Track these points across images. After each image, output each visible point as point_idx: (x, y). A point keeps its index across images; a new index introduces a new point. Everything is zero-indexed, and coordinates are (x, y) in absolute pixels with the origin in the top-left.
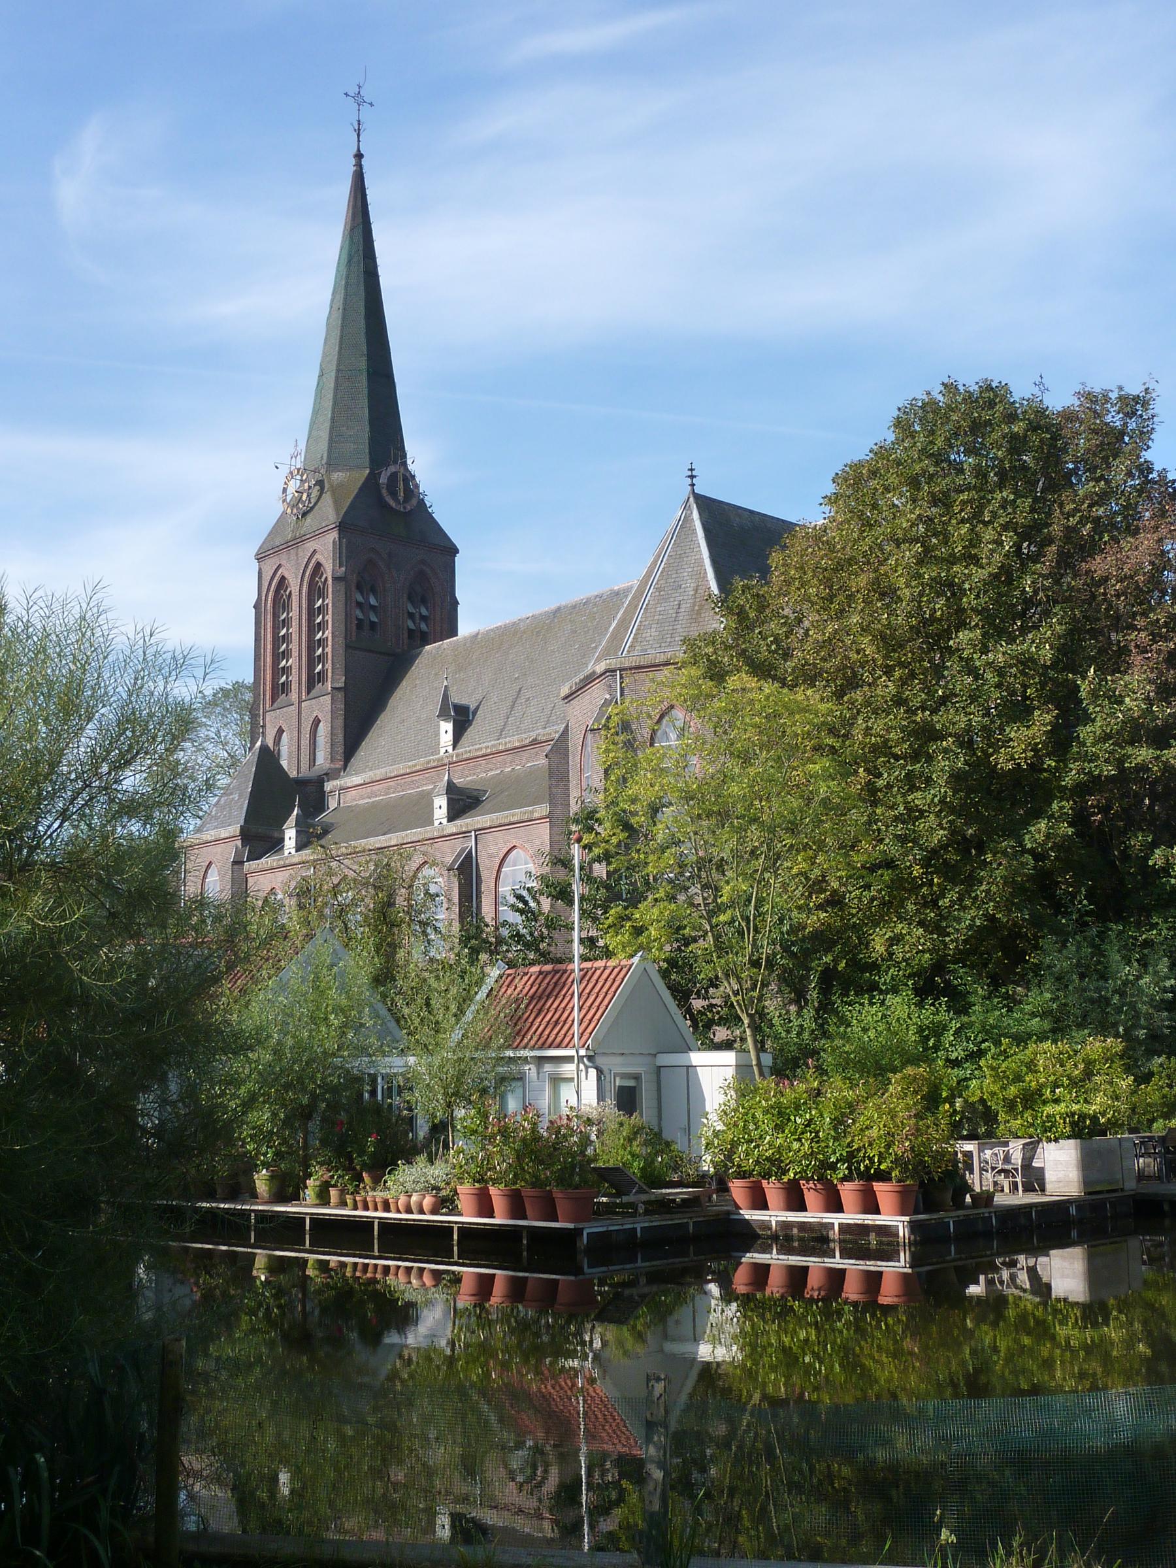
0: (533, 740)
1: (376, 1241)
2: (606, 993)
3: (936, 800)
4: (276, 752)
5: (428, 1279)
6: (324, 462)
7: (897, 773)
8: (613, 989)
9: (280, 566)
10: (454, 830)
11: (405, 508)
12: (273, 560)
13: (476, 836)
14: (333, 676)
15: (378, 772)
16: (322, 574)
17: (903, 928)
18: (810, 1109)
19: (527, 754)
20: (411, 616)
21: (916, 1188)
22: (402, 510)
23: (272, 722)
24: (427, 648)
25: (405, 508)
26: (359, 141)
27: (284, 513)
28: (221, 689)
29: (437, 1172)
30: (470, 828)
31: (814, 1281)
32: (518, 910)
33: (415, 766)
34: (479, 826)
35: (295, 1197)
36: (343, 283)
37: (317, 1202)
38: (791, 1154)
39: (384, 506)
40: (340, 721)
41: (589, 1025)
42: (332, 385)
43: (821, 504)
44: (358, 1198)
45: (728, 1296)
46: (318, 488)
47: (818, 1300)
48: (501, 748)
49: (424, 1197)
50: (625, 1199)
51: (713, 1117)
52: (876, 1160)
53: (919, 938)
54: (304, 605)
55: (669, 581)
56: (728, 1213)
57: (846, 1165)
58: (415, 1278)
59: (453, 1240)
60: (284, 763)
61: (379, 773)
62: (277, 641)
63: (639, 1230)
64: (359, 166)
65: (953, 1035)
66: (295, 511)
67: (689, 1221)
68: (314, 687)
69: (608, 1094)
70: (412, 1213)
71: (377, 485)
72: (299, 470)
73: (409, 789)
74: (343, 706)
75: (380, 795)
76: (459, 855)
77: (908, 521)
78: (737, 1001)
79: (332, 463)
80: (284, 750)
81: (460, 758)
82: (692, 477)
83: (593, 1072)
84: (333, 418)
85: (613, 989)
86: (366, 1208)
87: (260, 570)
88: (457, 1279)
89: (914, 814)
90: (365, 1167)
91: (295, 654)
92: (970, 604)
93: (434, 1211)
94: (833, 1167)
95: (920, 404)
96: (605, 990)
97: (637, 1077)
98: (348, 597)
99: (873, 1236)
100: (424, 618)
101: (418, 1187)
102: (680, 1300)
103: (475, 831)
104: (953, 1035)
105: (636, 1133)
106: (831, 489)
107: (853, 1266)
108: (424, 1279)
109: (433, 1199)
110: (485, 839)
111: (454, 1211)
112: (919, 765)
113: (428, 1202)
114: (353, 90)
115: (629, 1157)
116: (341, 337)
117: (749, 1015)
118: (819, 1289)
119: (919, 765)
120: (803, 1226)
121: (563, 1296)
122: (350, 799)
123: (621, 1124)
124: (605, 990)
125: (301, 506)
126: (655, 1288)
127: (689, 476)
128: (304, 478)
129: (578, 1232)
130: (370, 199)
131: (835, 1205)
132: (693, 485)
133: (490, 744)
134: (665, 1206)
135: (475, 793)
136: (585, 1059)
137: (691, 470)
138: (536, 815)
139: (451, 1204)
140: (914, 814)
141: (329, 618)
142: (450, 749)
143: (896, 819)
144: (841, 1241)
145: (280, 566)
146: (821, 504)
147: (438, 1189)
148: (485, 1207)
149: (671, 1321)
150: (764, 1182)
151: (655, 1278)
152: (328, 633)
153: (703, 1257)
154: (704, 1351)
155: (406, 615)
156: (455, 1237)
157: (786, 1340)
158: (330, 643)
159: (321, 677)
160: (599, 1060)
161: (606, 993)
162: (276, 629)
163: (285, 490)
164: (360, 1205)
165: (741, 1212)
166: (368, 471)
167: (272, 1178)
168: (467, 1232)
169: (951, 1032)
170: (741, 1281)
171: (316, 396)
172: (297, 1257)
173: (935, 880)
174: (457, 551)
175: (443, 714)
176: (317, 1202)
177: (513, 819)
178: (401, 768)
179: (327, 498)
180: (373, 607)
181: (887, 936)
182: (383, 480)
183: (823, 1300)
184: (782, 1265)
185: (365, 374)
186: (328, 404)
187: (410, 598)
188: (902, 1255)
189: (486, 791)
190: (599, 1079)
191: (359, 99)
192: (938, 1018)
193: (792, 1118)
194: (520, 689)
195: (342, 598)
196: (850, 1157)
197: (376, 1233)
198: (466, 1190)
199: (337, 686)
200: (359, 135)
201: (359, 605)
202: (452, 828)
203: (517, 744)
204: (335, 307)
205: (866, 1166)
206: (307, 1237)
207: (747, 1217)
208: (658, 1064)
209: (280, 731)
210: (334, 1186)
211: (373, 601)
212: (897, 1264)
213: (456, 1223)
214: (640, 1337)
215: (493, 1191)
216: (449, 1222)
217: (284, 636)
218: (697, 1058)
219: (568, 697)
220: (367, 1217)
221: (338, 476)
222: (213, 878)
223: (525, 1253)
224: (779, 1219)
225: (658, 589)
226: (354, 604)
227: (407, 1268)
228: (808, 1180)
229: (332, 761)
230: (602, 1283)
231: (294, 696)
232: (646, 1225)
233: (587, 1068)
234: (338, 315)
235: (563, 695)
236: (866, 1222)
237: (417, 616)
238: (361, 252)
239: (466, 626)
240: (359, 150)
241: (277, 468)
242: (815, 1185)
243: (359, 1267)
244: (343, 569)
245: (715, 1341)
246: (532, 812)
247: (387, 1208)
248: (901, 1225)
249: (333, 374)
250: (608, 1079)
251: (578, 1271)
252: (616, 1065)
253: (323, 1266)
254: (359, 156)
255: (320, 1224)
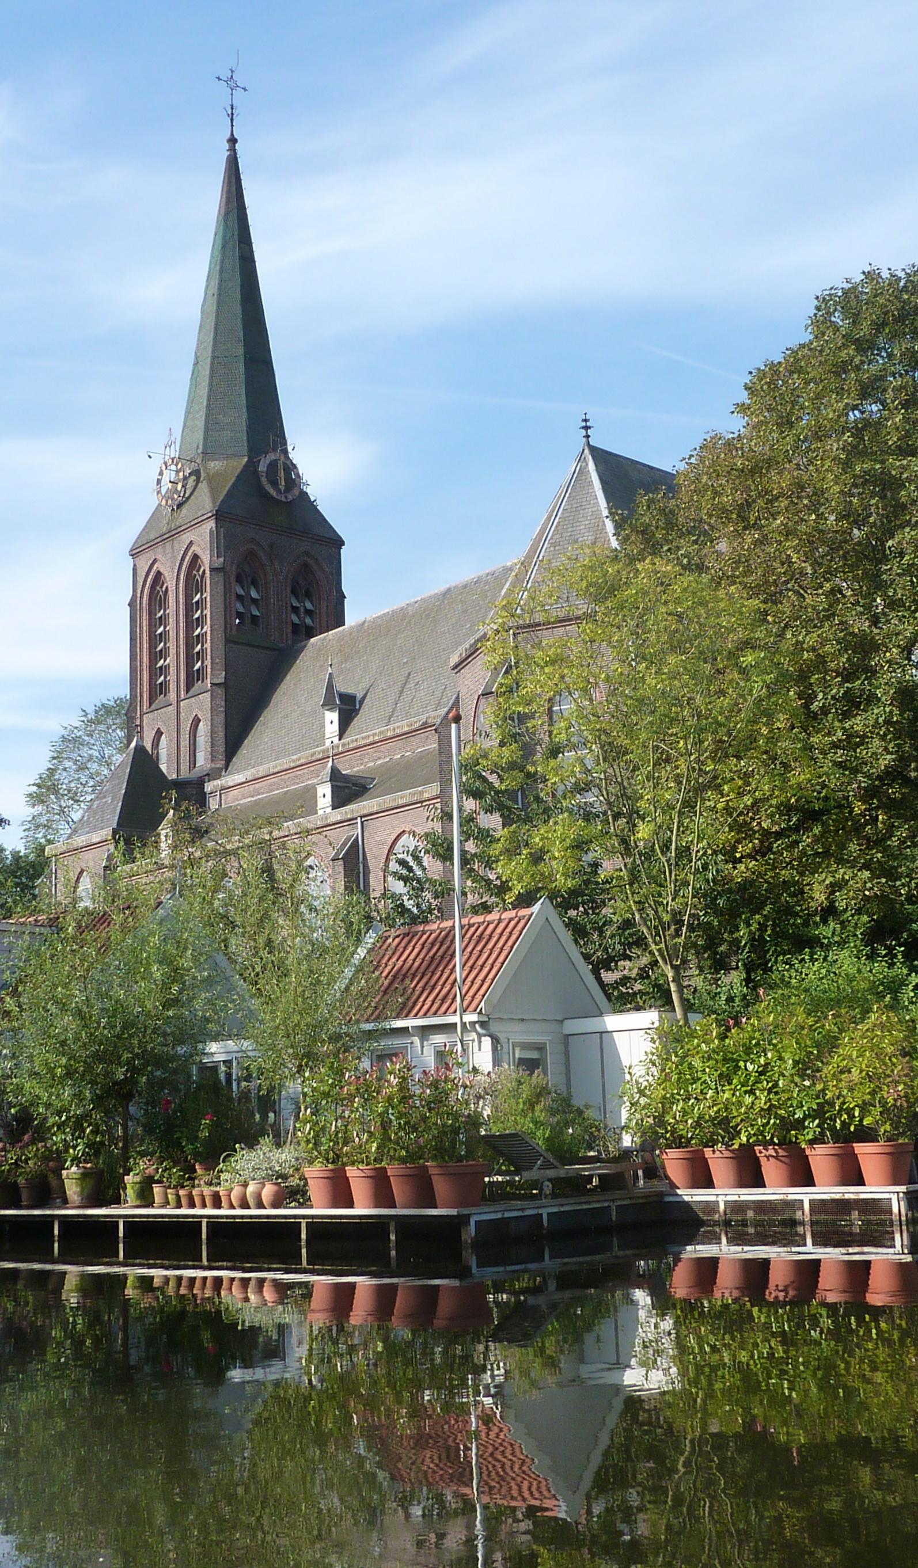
0: (423, 724)
1: (204, 1248)
2: (502, 949)
3: (881, 720)
4: (155, 755)
5: (269, 1294)
6: (200, 451)
7: (834, 691)
8: (510, 943)
9: (155, 561)
10: (339, 818)
11: (286, 497)
12: (148, 555)
13: (362, 823)
14: (213, 671)
15: (261, 768)
16: (200, 567)
17: (845, 873)
18: (764, 1051)
19: (415, 740)
20: (295, 610)
21: (911, 1148)
22: (283, 499)
23: (150, 724)
24: (312, 640)
25: (286, 497)
26: (232, 126)
27: (160, 505)
28: (103, 705)
29: (284, 1157)
30: (355, 815)
31: (778, 1277)
32: (401, 878)
33: (299, 759)
34: (366, 812)
35: (116, 1200)
36: (218, 268)
37: (138, 1203)
38: (743, 1110)
39: (266, 495)
40: (221, 719)
41: (482, 985)
42: (208, 373)
43: (733, 412)
44: (182, 1192)
45: (663, 1303)
46: (193, 478)
47: (784, 1304)
48: (389, 734)
49: (264, 1185)
50: (527, 1175)
51: (639, 1071)
52: (857, 1114)
53: (865, 882)
54: (182, 600)
55: (565, 535)
56: (662, 1194)
57: (817, 1121)
58: (255, 1293)
59: (300, 1240)
60: (163, 768)
61: (262, 770)
62: (155, 639)
63: (545, 1216)
64: (233, 150)
65: (912, 991)
66: (170, 502)
67: (612, 1204)
68: (193, 685)
69: (505, 1057)
70: (249, 1207)
71: (256, 471)
72: (173, 459)
73: (293, 784)
74: (223, 703)
75: (263, 792)
76: (344, 844)
77: (834, 411)
78: (659, 950)
79: (207, 454)
80: (163, 752)
81: (347, 748)
82: (586, 428)
83: (487, 1042)
84: (208, 406)
85: (510, 943)
86: (192, 1205)
87: (135, 565)
88: (307, 1288)
89: (853, 741)
90: (197, 1156)
91: (173, 651)
92: (909, 496)
93: (275, 1205)
94: (799, 1125)
95: (840, 294)
96: (500, 945)
97: (540, 1048)
98: (227, 589)
99: (855, 1214)
100: (308, 612)
101: (258, 1174)
102: (601, 1310)
103: (361, 817)
104: (912, 991)
105: (539, 1095)
106: (747, 379)
107: (831, 1255)
108: (265, 1294)
109: (275, 1188)
110: (371, 825)
111: (306, 1203)
112: (860, 682)
113: (268, 1192)
114: (226, 75)
115: (531, 1125)
116: (216, 324)
117: (673, 966)
118: (785, 1290)
119: (860, 682)
120: (761, 1207)
121: (445, 1306)
122: (235, 799)
123: (520, 1083)
124: (500, 945)
125: (176, 496)
126: (568, 1294)
127: (583, 428)
128: (179, 466)
129: (462, 1220)
130: (244, 184)
131: (804, 1176)
132: (588, 436)
133: (377, 731)
134: (576, 1186)
135: (362, 781)
136: (477, 1026)
137: (586, 421)
138: (426, 796)
139: (303, 1196)
140: (853, 741)
141: (207, 612)
142: (336, 740)
143: (835, 746)
144: (813, 1223)
145: (155, 561)
146: (733, 412)
147: (285, 1177)
148: (342, 1195)
149: (589, 1338)
150: (708, 1152)
151: (567, 1280)
152: (207, 628)
153: (629, 1252)
154: (632, 1377)
155: (289, 608)
156: (304, 1236)
157: (743, 1356)
158: (209, 638)
159: (200, 675)
160: (494, 1027)
161: (502, 949)
162: (152, 626)
163: (159, 482)
164: (184, 1201)
165: (679, 1192)
166: (246, 459)
167: (85, 1175)
168: (320, 1229)
169: (911, 987)
170: (680, 1285)
171: (191, 385)
172: (108, 1274)
173: (880, 817)
174: (342, 543)
175: (328, 703)
176: (138, 1203)
177: (401, 802)
178: (284, 763)
179: (203, 486)
180: (254, 601)
181: (827, 882)
182: (262, 468)
183: (790, 1303)
184: (734, 1260)
185: (242, 360)
186: (204, 391)
187: (294, 592)
188: (897, 1236)
189: (373, 779)
190: (495, 1049)
191: (231, 83)
192: (892, 973)
193: (742, 1064)
194: (409, 674)
195: (221, 588)
196: (819, 1113)
197: (204, 1236)
198: (315, 1173)
199: (217, 681)
200: (232, 120)
201: (239, 597)
202: (337, 815)
203: (406, 729)
204: (210, 293)
205: (843, 1123)
206: (121, 1246)
207: (687, 1198)
208: (566, 1032)
209: (159, 733)
210: (159, 1182)
211: (254, 594)
212: (891, 1250)
213: (304, 1217)
214: (552, 1363)
215: (351, 1171)
216: (295, 1217)
217: (161, 634)
218: (613, 1021)
219: (458, 667)
220: (193, 1216)
221: (215, 465)
222: (86, 885)
223: (393, 1253)
224: (729, 1198)
225: (554, 545)
226: (233, 597)
227: (242, 1279)
228: (766, 1144)
229: (212, 761)
230: (498, 1289)
231: (172, 696)
232: (555, 1210)
233: (480, 1036)
234: (213, 302)
235: (452, 664)
236: (847, 1196)
237: (302, 610)
238: (236, 237)
239: (353, 616)
240: (232, 134)
241: (150, 457)
242: (776, 1151)
243: (184, 1283)
244: (222, 560)
245: (648, 1365)
246: (421, 793)
247: (217, 1203)
248: (894, 1197)
249: (209, 360)
250: (505, 1050)
251: (463, 1273)
252: (515, 1034)
253: (146, 1283)
254: (233, 141)
255: (137, 1228)
